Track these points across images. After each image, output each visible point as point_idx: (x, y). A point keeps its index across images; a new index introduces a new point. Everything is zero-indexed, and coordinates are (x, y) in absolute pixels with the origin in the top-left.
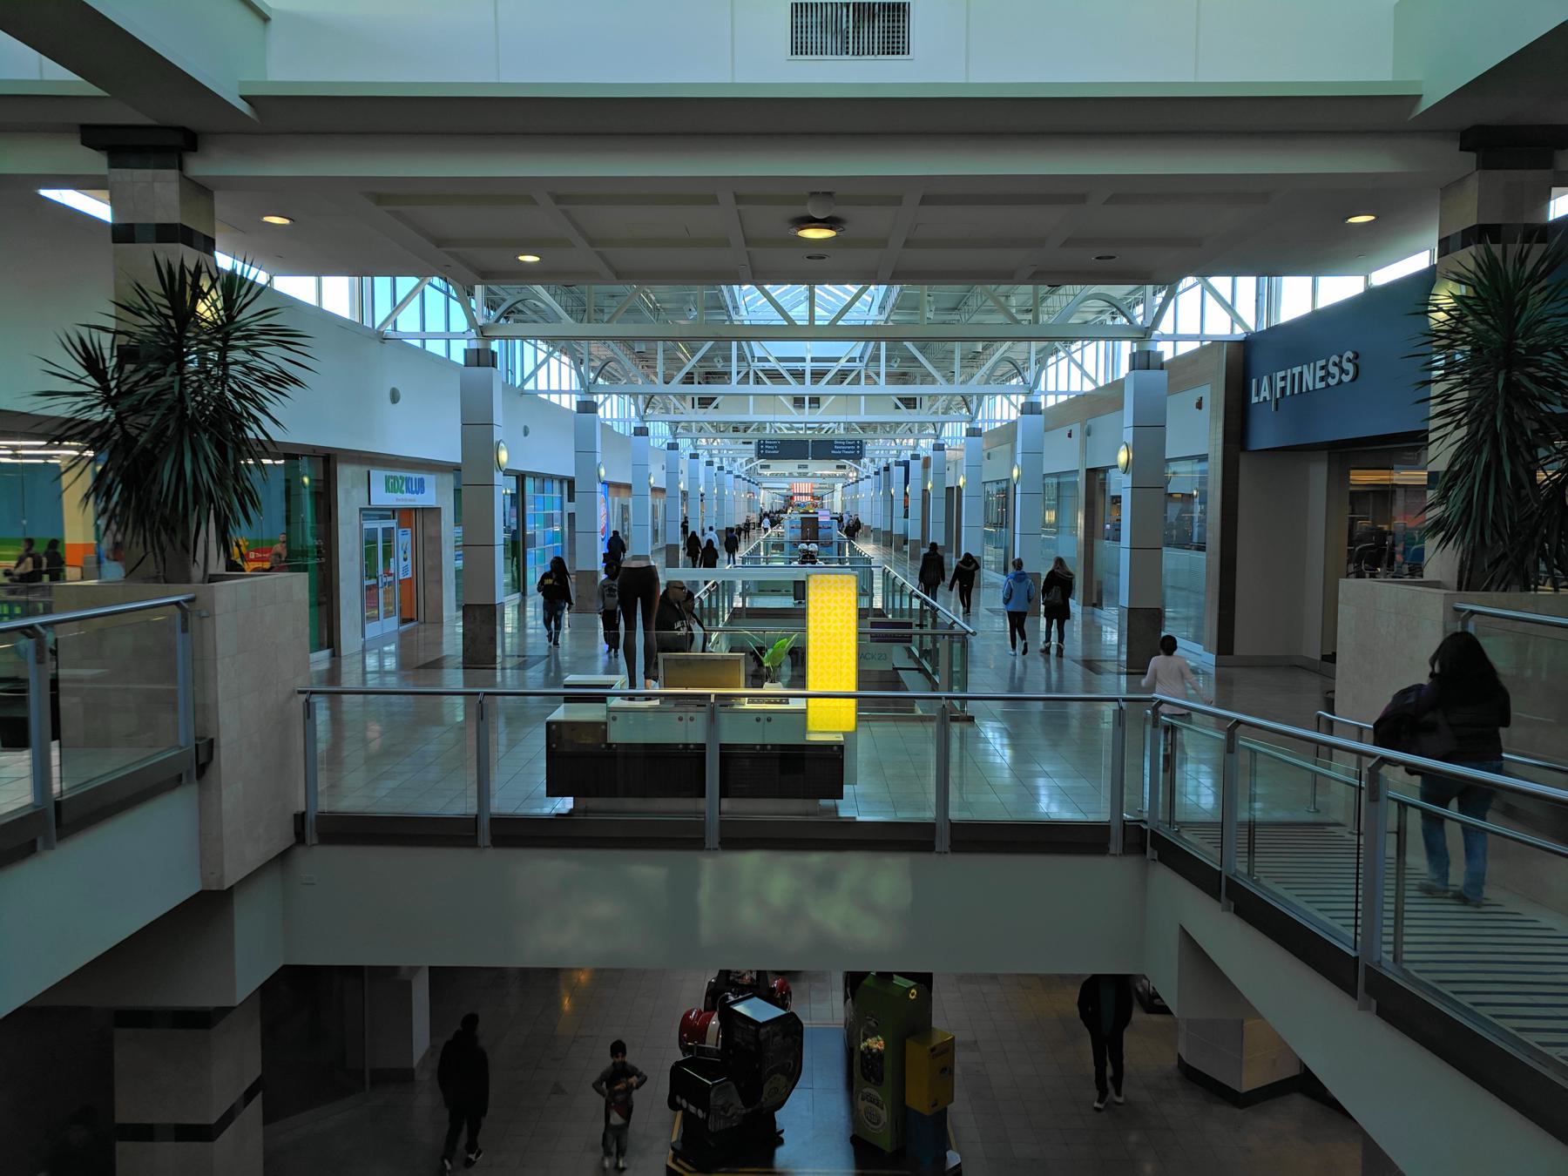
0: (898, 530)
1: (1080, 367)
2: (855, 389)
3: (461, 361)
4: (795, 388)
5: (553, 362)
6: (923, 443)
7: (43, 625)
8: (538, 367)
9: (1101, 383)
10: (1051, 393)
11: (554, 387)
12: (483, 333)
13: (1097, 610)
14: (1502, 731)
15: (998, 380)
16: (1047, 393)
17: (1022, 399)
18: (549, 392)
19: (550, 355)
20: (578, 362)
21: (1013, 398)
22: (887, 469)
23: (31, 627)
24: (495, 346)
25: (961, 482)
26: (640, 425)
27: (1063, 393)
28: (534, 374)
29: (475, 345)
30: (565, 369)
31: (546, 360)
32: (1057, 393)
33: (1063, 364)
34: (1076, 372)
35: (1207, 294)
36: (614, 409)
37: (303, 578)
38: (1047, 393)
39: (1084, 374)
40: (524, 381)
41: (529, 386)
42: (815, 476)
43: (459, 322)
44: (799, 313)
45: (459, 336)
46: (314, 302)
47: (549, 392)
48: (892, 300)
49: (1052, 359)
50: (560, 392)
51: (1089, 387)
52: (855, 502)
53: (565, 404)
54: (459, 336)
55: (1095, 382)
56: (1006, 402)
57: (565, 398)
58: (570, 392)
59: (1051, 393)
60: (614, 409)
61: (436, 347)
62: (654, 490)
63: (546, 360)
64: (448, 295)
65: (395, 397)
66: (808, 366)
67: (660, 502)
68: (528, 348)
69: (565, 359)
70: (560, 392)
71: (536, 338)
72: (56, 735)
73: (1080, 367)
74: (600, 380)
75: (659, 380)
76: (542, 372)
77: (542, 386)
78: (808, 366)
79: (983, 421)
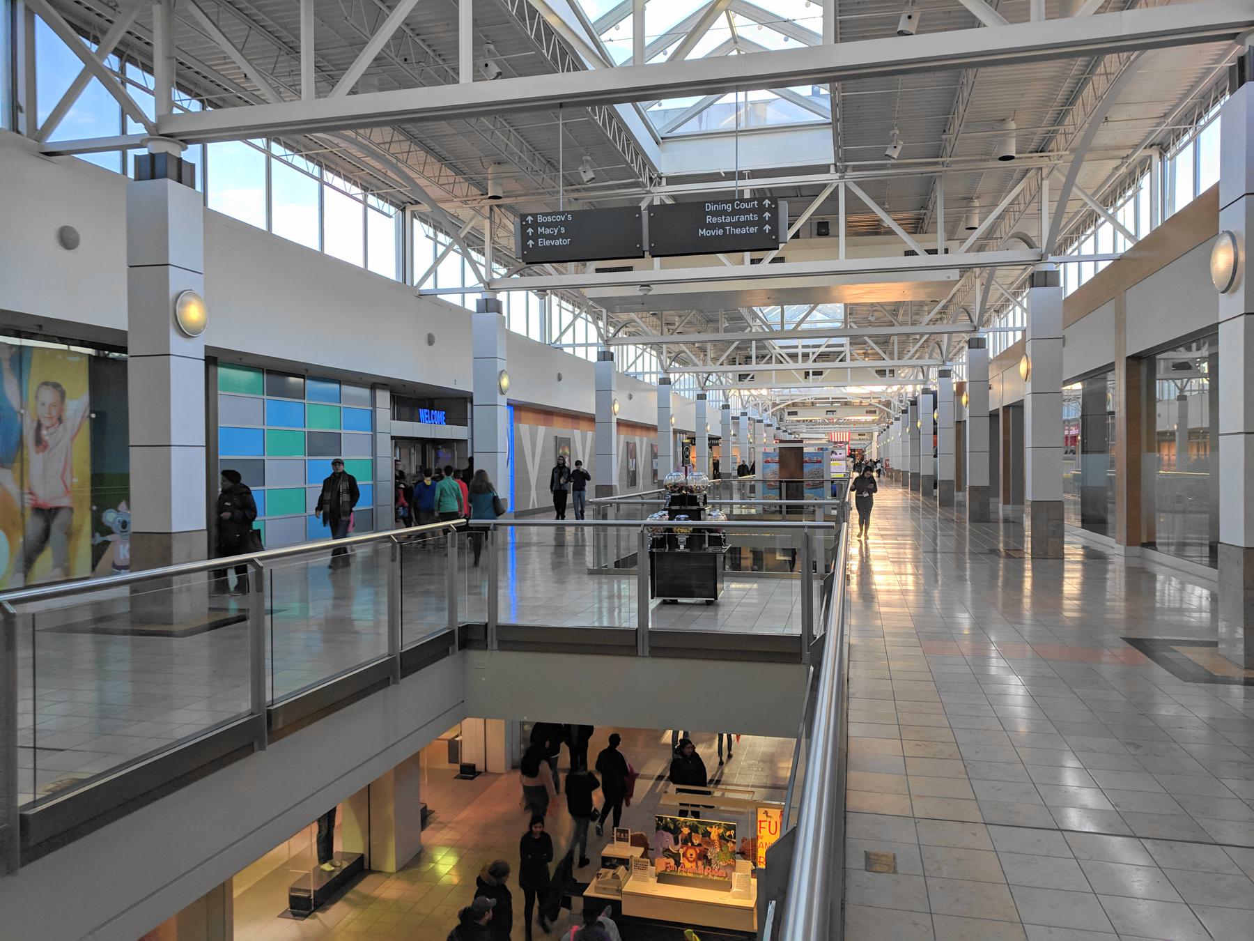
0: (926, 470)
2: (842, 364)
3: (474, 309)
4: (800, 364)
5: (647, 355)
7: (261, 559)
8: (637, 358)
9: (1145, 232)
11: (647, 369)
12: (607, 342)
13: (1150, 552)
18: (644, 373)
19: (644, 350)
22: (914, 403)
23: (389, 537)
24: (612, 349)
26: (488, 295)
28: (635, 362)
29: (604, 349)
30: (654, 359)
31: (572, 324)
33: (1018, 309)
36: (684, 383)
37: (1159, 428)
39: (1119, 227)
42: (849, 422)
43: (472, 280)
45: (473, 290)
47: (574, 345)
51: (1124, 246)
52: (886, 447)
54: (473, 290)
61: (580, 352)
62: (620, 423)
65: (560, 378)
66: (800, 351)
67: (642, 442)
68: (632, 348)
69: (654, 353)
71: (528, 289)
78: (800, 351)
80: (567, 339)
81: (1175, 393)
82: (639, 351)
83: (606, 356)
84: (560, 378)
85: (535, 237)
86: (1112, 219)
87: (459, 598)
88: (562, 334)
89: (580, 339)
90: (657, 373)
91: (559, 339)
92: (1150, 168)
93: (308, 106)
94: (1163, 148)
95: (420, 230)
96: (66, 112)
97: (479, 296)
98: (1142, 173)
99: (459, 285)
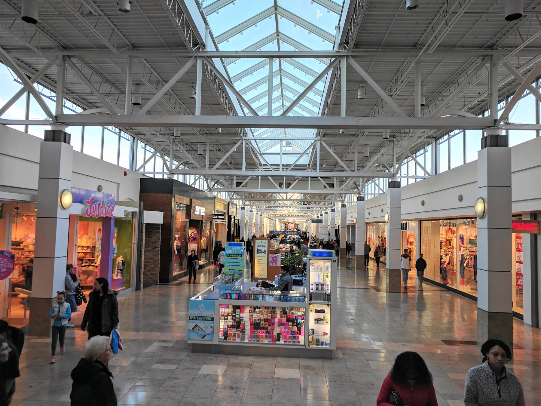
27: (412, 177)
34: (377, 188)
35: (417, 165)
64: (145, 150)
73: (378, 186)
83: (57, 136)
84: (125, 174)
88: (146, 162)
91: (143, 166)
92: (431, 143)
93: (207, 171)
94: (437, 139)
95: (140, 145)
97: (49, 128)
98: (429, 145)
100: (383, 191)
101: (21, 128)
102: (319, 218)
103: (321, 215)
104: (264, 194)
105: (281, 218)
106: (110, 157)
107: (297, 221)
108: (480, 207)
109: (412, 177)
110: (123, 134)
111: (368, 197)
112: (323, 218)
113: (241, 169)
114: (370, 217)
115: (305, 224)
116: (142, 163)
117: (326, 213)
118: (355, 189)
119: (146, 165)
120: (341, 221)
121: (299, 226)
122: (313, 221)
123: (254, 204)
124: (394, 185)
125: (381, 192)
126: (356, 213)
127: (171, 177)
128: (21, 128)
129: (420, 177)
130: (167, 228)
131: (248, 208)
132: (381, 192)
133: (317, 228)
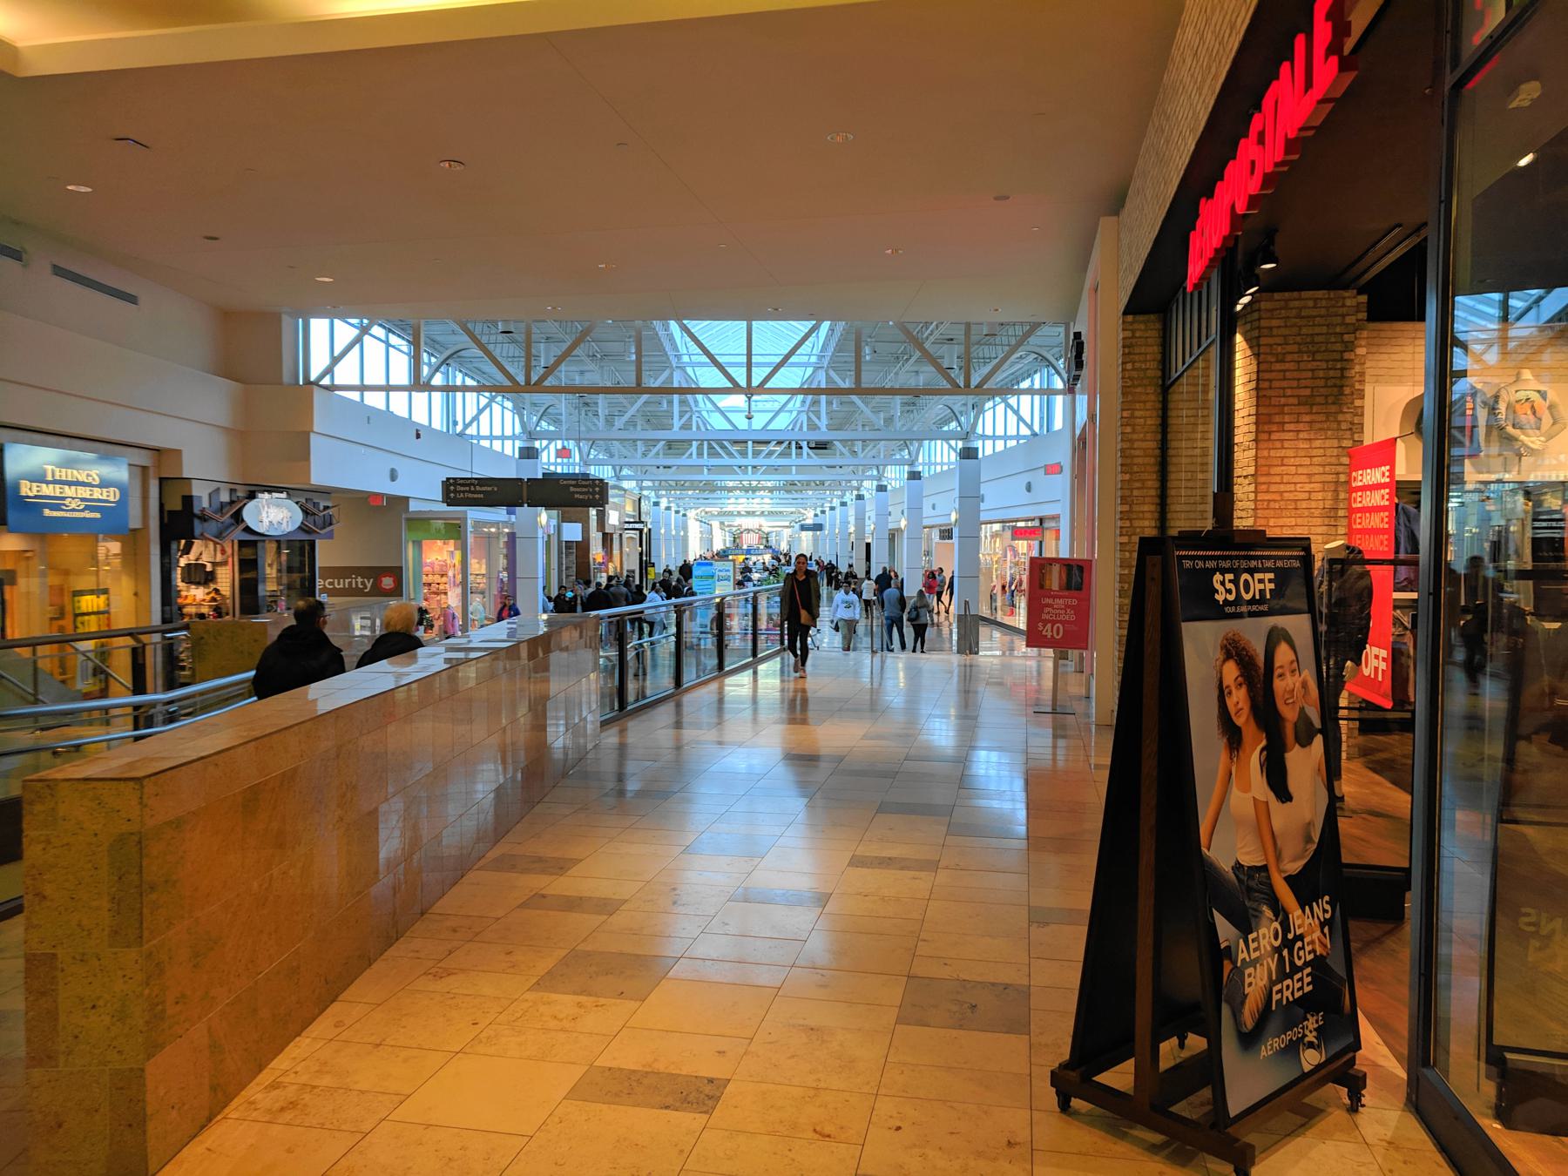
1: (1016, 412)
5: (496, 408)
6: (866, 484)
8: (480, 411)
10: (1000, 438)
11: (497, 432)
14: (414, 506)
15: (936, 433)
16: (984, 437)
17: (960, 444)
18: (491, 438)
19: (492, 400)
20: (518, 410)
21: (953, 443)
24: (537, 444)
25: (903, 523)
27: (1011, 438)
28: (476, 418)
30: (508, 415)
31: (488, 405)
32: (942, 464)
34: (1012, 418)
38: (984, 437)
40: (466, 426)
41: (472, 431)
44: (742, 423)
46: (336, 321)
47: (491, 438)
48: (837, 334)
49: (989, 404)
50: (503, 438)
53: (508, 451)
55: (1008, 406)
56: (946, 446)
57: (508, 443)
58: (513, 437)
59: (1000, 438)
60: (941, 733)
63: (488, 405)
64: (388, 345)
69: (509, 404)
70: (503, 438)
72: (868, 545)
73: (1016, 412)
74: (544, 424)
75: (601, 423)
76: (470, 414)
77: (485, 431)
79: (924, 464)
80: (472, 431)
81: (746, 691)
82: (483, 401)
84: (418, 436)
85: (455, 492)
86: (645, 565)
87: (1446, 814)
88: (335, 360)
89: (375, 377)
90: (513, 437)
91: (329, 371)
96: (1113, 704)
99: (383, 382)
100: (1030, 427)
101: (354, 396)
102: (818, 521)
103: (823, 512)
104: (708, 483)
105: (723, 519)
106: (420, 417)
107: (766, 525)
108: (953, 517)
109: (1011, 438)
110: (393, 339)
111: (986, 449)
112: (826, 520)
113: (670, 428)
114: (933, 513)
115: (786, 533)
116: (326, 362)
117: (844, 504)
118: (947, 422)
119: (337, 369)
120: (961, 511)
121: (773, 539)
122: (803, 528)
123: (648, 476)
124: (968, 454)
125: (1025, 431)
126: (956, 493)
127: (583, 470)
128: (354, 396)
129: (1024, 437)
130: (582, 547)
131: (664, 503)
132: (1025, 431)
133: (815, 540)
